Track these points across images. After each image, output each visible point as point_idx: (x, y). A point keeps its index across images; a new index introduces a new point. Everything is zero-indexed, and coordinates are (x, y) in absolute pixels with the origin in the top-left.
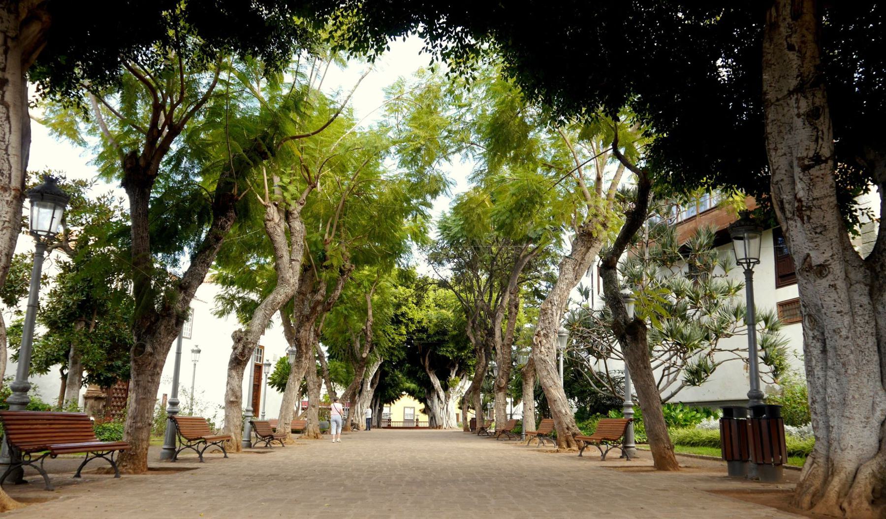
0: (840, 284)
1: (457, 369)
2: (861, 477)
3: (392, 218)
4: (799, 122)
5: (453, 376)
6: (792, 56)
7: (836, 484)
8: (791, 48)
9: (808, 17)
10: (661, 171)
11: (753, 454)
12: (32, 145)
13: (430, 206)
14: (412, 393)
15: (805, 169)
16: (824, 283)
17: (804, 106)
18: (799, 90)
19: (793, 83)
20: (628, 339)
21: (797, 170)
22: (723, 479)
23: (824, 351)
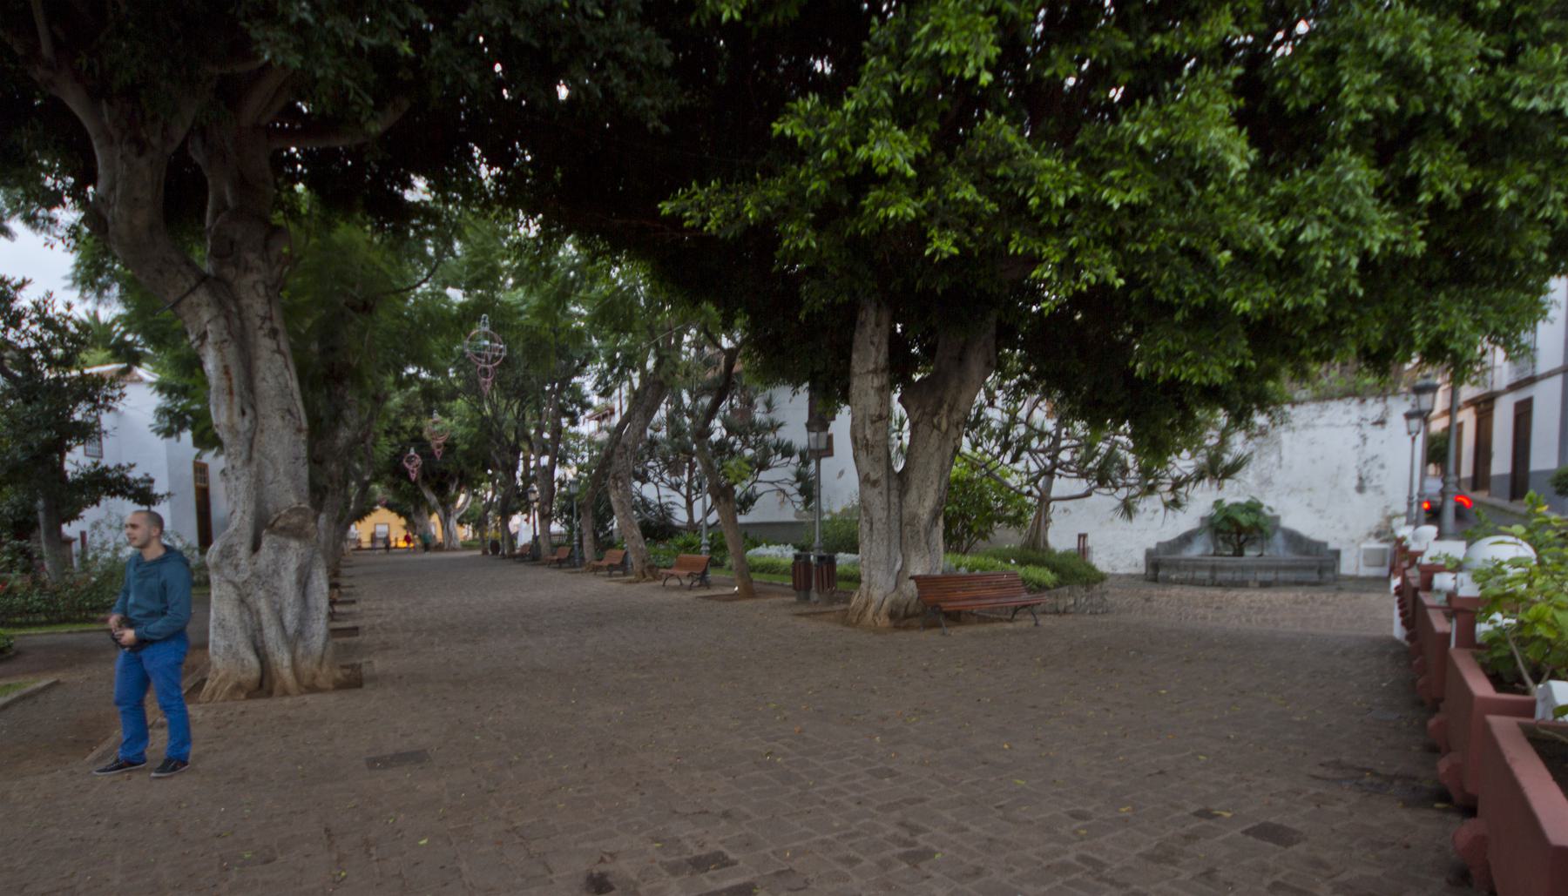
0: (885, 492)
1: (457, 483)
2: (886, 603)
3: (990, 520)
4: (872, 392)
5: (453, 491)
6: (872, 349)
7: (872, 607)
8: (872, 343)
9: (885, 326)
10: (415, 299)
11: (818, 583)
12: (1550, 778)
13: (774, 427)
14: (390, 507)
15: (873, 422)
16: (877, 491)
17: (876, 383)
18: (875, 372)
19: (871, 367)
20: (722, 500)
21: (868, 422)
22: (796, 604)
23: (871, 529)
